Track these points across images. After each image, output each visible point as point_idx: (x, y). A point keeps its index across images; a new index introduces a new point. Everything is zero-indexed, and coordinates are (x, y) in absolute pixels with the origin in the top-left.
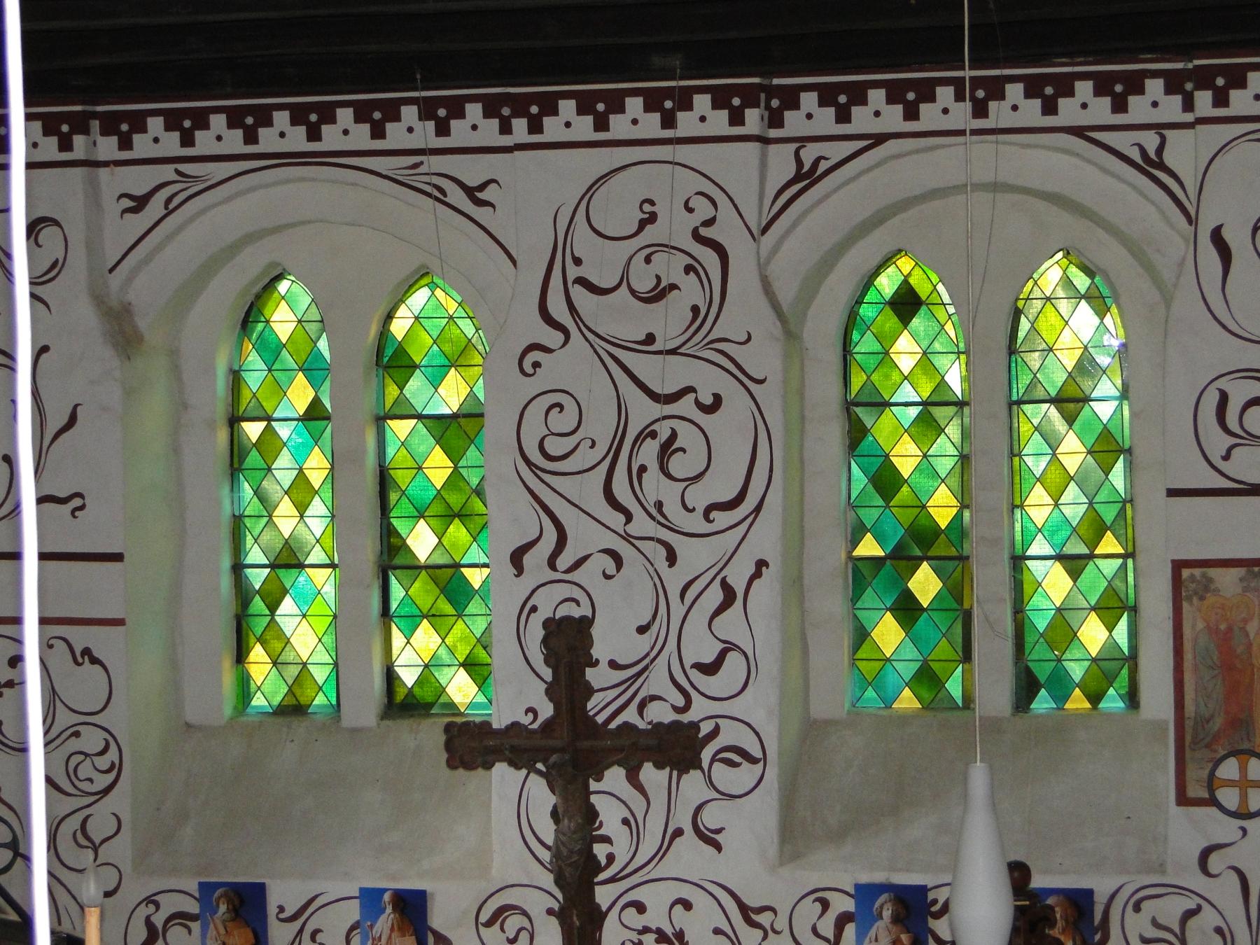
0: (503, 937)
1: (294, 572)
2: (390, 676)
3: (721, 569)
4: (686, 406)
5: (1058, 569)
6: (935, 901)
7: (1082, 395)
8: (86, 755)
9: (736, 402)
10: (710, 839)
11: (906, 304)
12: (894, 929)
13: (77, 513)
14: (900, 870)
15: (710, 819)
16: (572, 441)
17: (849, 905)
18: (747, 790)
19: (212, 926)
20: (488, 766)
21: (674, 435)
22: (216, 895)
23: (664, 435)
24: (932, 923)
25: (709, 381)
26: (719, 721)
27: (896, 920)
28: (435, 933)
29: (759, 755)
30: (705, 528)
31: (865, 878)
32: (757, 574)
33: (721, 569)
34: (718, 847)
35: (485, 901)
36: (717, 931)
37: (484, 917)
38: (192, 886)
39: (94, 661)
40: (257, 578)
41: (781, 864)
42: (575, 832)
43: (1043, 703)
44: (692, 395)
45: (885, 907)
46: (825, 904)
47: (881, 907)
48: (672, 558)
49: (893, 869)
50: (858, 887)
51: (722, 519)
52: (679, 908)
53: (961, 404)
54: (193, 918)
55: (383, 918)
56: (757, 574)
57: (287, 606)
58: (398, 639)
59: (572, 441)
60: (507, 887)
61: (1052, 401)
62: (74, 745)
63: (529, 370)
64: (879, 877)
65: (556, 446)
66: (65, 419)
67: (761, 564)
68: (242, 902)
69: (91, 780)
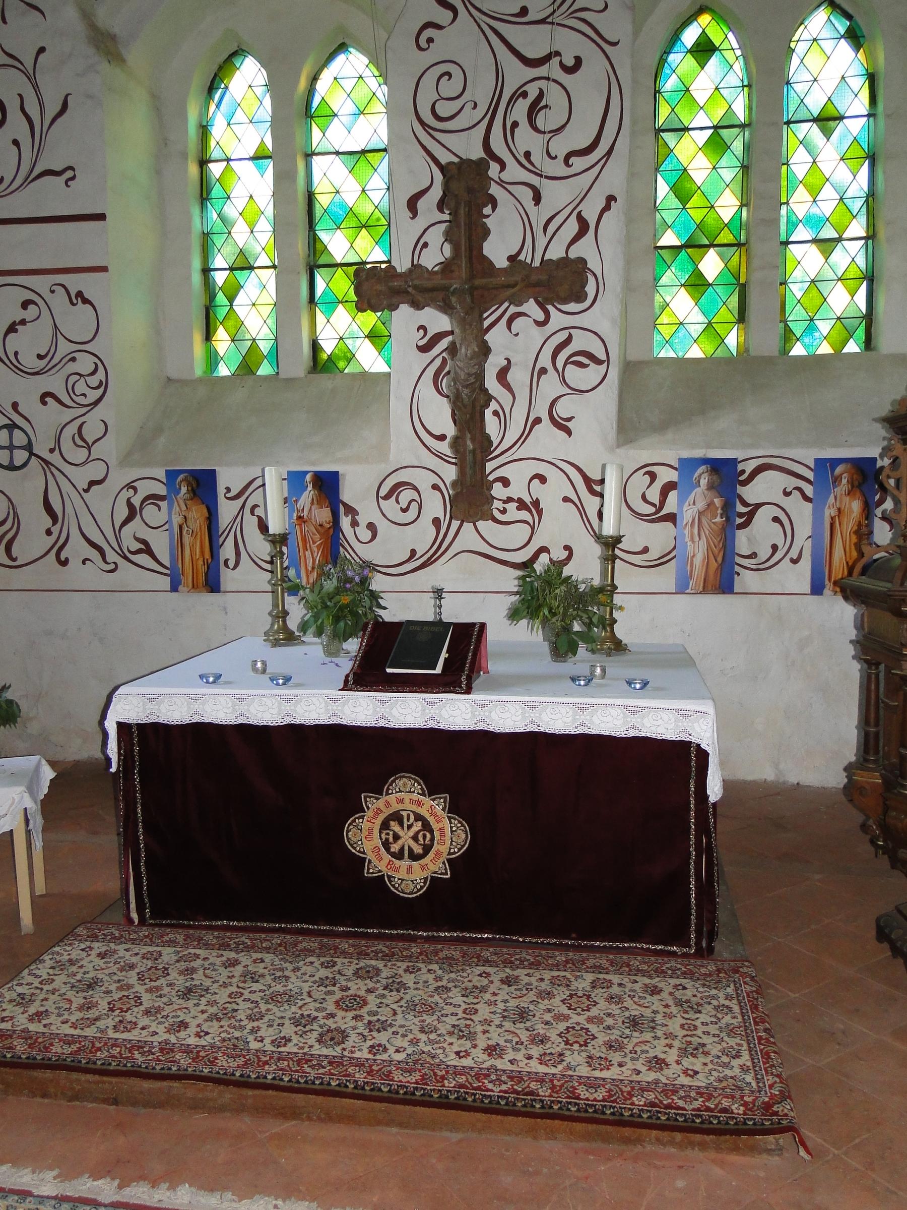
0: (399, 507)
1: (247, 272)
2: (315, 347)
3: (578, 205)
4: (553, 69)
5: (813, 249)
6: (743, 472)
7: (838, 115)
8: (81, 375)
9: (594, 64)
10: (562, 426)
11: (704, 50)
12: (709, 494)
13: (69, 183)
14: (713, 448)
15: (562, 410)
16: (455, 105)
17: (673, 476)
18: (593, 386)
19: (176, 503)
20: (393, 308)
21: (541, 95)
22: (178, 480)
23: (533, 94)
24: (740, 490)
25: (570, 44)
26: (572, 331)
27: (710, 487)
28: (345, 505)
29: (603, 357)
30: (563, 171)
31: (686, 454)
32: (607, 208)
33: (578, 205)
34: (569, 432)
35: (385, 479)
36: (566, 499)
37: (383, 492)
38: (161, 474)
39: (86, 301)
40: (220, 278)
41: (618, 446)
42: (471, 359)
43: (798, 350)
44: (558, 59)
45: (703, 476)
46: (653, 476)
47: (700, 476)
48: (537, 198)
49: (709, 446)
50: (681, 460)
51: (579, 163)
52: (536, 481)
53: (743, 126)
54: (162, 498)
55: (306, 493)
56: (607, 208)
57: (240, 299)
58: (320, 318)
59: (455, 105)
60: (401, 468)
61: (815, 120)
62: (72, 367)
63: (423, 44)
64: (698, 453)
65: (444, 109)
66: (59, 107)
67: (611, 199)
68: (198, 485)
69: (84, 395)
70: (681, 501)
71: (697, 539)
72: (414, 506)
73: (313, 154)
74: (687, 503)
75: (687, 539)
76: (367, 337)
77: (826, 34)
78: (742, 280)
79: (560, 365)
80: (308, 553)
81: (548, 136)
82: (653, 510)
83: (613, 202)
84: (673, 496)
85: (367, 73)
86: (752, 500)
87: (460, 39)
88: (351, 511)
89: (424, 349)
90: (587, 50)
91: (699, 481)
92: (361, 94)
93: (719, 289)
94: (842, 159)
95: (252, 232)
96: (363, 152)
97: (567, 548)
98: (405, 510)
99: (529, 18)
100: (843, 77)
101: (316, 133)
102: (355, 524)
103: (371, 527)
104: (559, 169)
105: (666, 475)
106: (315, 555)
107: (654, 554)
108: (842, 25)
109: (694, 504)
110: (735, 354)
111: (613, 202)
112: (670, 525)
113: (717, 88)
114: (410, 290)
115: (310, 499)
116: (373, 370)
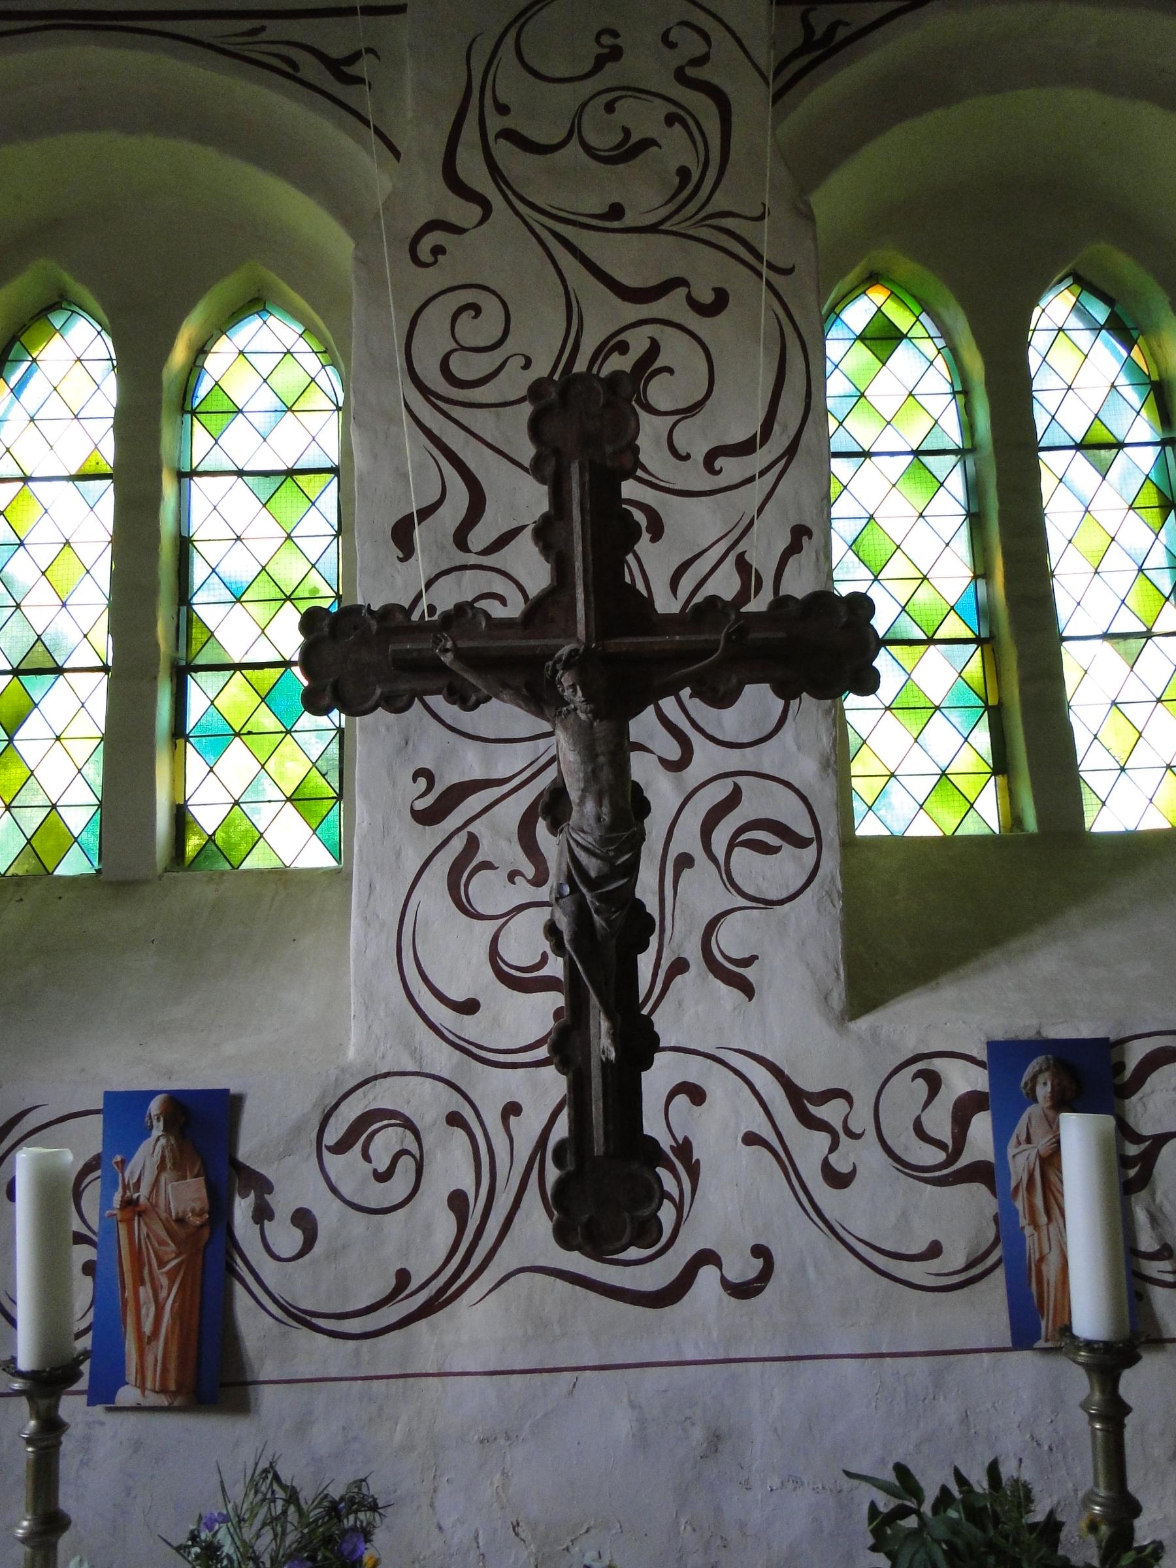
0: (368, 1168)
2: (181, 817)
4: (672, 306)
10: (735, 976)
11: (883, 338)
17: (978, 1080)
21: (654, 348)
25: (706, 270)
26: (742, 781)
29: (807, 831)
30: (707, 482)
32: (794, 548)
34: (748, 989)
36: (751, 1139)
44: (681, 292)
45: (1041, 1079)
47: (1034, 1079)
51: (732, 468)
52: (682, 1100)
55: (146, 1147)
56: (794, 548)
58: (195, 764)
59: (482, 365)
70: (1001, 1135)
71: (1043, 1219)
72: (406, 1165)
73: (194, 473)
74: (1013, 1140)
75: (1023, 1221)
76: (289, 799)
77: (1074, 322)
78: (992, 701)
79: (719, 850)
80: (145, 1292)
81: (671, 420)
82: (941, 1156)
83: (805, 539)
84: (981, 1126)
85: (302, 345)
86: (1147, 1129)
87: (496, 251)
88: (261, 1185)
89: (427, 817)
90: (737, 280)
91: (1033, 1090)
92: (289, 379)
93: (954, 715)
94: (1131, 508)
95: (64, 605)
96: (291, 473)
97: (759, 1251)
98: (383, 1177)
99: (629, 220)
100: (1113, 386)
101: (201, 440)
102: (263, 1213)
103: (304, 1219)
104: (694, 476)
105: (963, 1080)
106: (163, 1294)
107: (955, 1257)
108: (1100, 312)
109: (1028, 1140)
110: (997, 832)
111: (805, 539)
112: (979, 1190)
113: (911, 394)
114: (447, 659)
115: (157, 1158)
116: (301, 864)
